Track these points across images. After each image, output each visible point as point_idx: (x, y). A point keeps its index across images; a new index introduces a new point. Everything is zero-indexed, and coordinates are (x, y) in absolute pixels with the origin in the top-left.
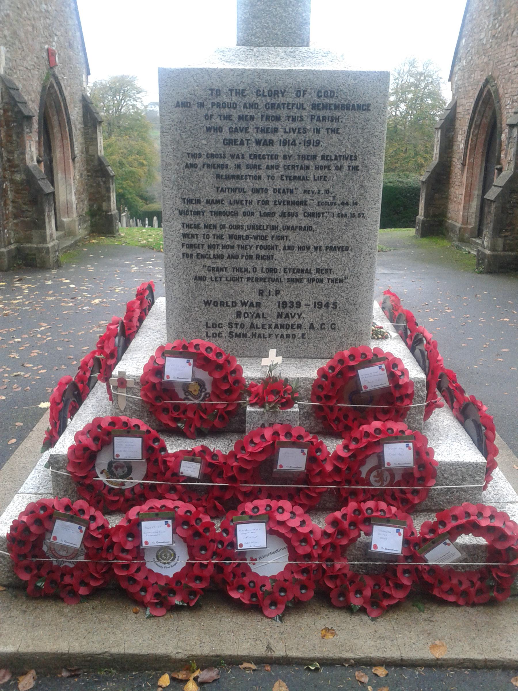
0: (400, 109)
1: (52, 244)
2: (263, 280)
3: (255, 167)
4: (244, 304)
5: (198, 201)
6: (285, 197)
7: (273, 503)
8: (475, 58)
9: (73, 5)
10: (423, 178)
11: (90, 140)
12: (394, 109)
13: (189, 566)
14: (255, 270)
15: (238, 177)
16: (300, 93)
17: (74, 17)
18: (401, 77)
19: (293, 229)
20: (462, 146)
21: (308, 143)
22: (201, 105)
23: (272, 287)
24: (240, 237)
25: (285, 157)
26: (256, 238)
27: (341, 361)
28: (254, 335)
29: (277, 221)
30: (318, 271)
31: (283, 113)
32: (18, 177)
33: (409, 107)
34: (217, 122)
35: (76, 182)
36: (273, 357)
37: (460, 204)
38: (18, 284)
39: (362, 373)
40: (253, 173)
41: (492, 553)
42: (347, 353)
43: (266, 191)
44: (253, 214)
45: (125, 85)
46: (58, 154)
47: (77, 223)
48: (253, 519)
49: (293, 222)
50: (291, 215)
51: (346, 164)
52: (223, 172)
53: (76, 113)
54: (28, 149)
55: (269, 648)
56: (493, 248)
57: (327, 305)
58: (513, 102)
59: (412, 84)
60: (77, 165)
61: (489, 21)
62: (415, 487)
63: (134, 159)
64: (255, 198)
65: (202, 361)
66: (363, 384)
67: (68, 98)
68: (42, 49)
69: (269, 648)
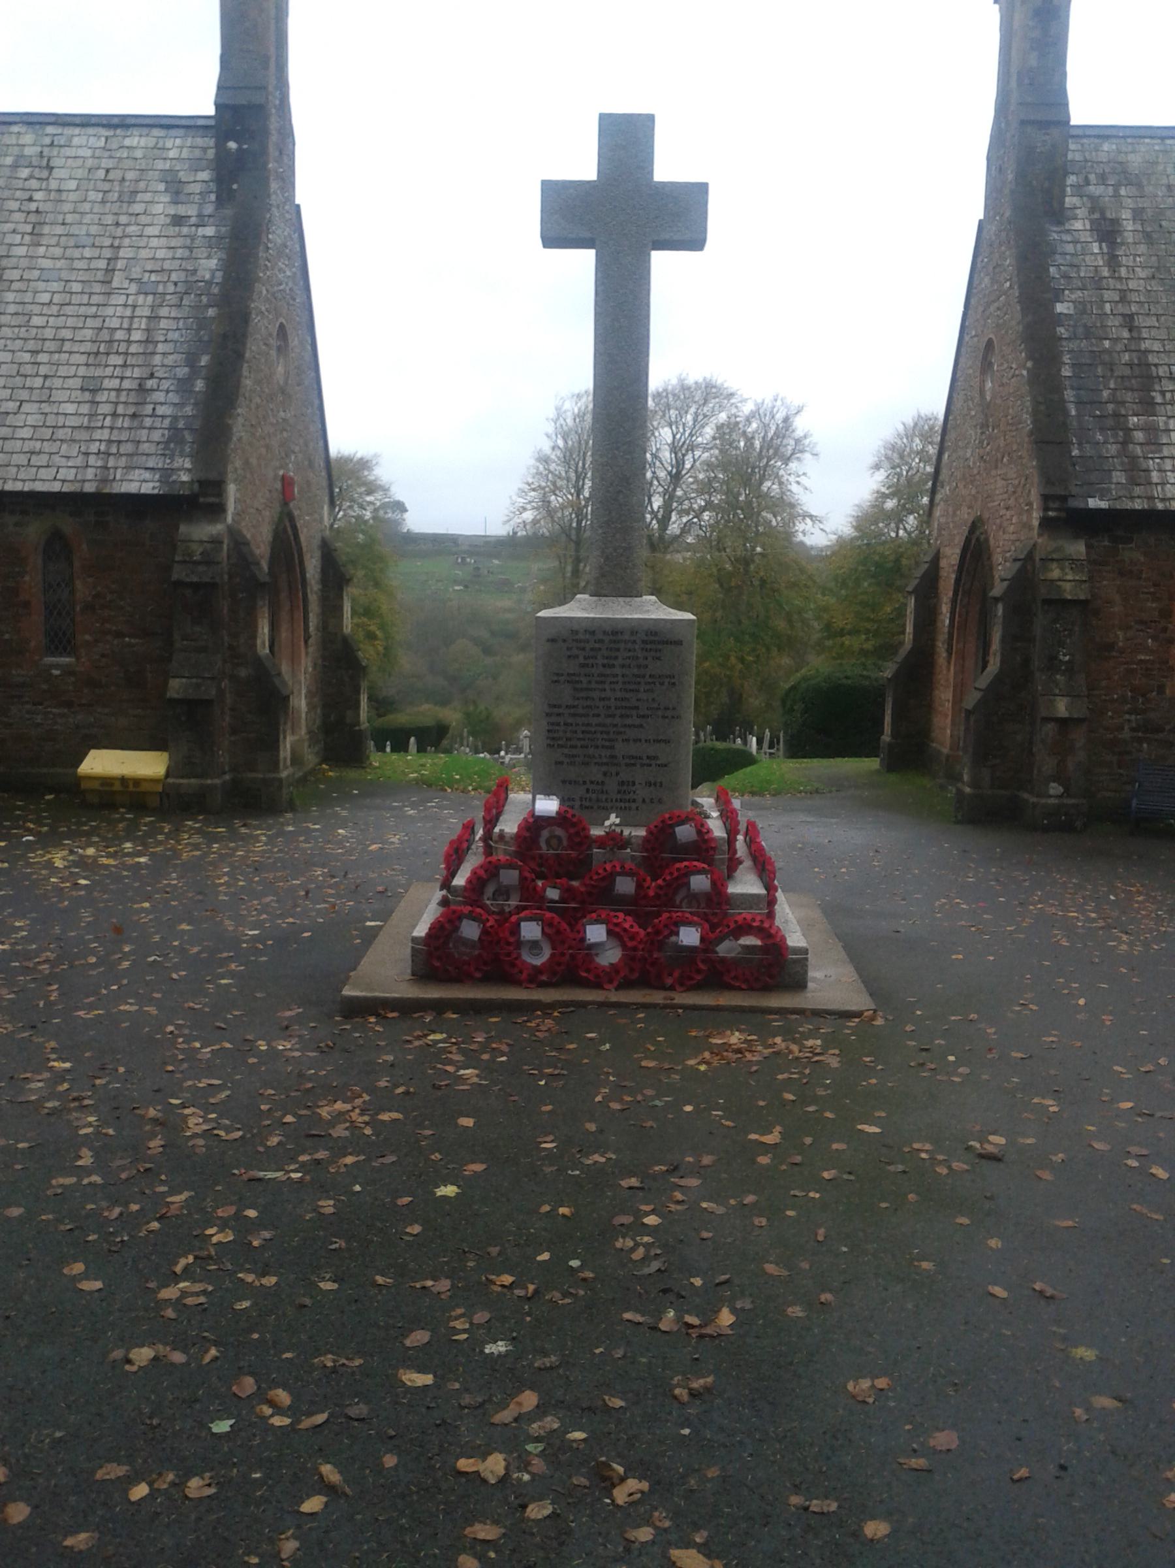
2: (606, 764)
3: (602, 682)
4: (592, 782)
5: (560, 707)
6: (624, 704)
7: (612, 914)
8: (961, 486)
11: (331, 608)
12: (893, 525)
13: (552, 955)
14: (600, 756)
15: (591, 690)
16: (634, 632)
18: (907, 463)
20: (947, 621)
21: (639, 667)
22: (564, 641)
23: (613, 770)
27: (663, 822)
28: (599, 807)
29: (617, 720)
31: (622, 646)
32: (243, 673)
34: (575, 652)
36: (613, 819)
37: (946, 716)
38: (243, 830)
39: (678, 830)
40: (600, 686)
41: (765, 949)
42: (667, 816)
43: (609, 699)
46: (284, 634)
47: (306, 744)
48: (597, 921)
49: (629, 721)
50: (628, 716)
51: (667, 680)
52: (579, 686)
53: (312, 566)
54: (260, 630)
56: (974, 784)
57: (655, 784)
60: (311, 650)
62: (716, 910)
64: (601, 704)
67: (304, 544)
68: (276, 476)
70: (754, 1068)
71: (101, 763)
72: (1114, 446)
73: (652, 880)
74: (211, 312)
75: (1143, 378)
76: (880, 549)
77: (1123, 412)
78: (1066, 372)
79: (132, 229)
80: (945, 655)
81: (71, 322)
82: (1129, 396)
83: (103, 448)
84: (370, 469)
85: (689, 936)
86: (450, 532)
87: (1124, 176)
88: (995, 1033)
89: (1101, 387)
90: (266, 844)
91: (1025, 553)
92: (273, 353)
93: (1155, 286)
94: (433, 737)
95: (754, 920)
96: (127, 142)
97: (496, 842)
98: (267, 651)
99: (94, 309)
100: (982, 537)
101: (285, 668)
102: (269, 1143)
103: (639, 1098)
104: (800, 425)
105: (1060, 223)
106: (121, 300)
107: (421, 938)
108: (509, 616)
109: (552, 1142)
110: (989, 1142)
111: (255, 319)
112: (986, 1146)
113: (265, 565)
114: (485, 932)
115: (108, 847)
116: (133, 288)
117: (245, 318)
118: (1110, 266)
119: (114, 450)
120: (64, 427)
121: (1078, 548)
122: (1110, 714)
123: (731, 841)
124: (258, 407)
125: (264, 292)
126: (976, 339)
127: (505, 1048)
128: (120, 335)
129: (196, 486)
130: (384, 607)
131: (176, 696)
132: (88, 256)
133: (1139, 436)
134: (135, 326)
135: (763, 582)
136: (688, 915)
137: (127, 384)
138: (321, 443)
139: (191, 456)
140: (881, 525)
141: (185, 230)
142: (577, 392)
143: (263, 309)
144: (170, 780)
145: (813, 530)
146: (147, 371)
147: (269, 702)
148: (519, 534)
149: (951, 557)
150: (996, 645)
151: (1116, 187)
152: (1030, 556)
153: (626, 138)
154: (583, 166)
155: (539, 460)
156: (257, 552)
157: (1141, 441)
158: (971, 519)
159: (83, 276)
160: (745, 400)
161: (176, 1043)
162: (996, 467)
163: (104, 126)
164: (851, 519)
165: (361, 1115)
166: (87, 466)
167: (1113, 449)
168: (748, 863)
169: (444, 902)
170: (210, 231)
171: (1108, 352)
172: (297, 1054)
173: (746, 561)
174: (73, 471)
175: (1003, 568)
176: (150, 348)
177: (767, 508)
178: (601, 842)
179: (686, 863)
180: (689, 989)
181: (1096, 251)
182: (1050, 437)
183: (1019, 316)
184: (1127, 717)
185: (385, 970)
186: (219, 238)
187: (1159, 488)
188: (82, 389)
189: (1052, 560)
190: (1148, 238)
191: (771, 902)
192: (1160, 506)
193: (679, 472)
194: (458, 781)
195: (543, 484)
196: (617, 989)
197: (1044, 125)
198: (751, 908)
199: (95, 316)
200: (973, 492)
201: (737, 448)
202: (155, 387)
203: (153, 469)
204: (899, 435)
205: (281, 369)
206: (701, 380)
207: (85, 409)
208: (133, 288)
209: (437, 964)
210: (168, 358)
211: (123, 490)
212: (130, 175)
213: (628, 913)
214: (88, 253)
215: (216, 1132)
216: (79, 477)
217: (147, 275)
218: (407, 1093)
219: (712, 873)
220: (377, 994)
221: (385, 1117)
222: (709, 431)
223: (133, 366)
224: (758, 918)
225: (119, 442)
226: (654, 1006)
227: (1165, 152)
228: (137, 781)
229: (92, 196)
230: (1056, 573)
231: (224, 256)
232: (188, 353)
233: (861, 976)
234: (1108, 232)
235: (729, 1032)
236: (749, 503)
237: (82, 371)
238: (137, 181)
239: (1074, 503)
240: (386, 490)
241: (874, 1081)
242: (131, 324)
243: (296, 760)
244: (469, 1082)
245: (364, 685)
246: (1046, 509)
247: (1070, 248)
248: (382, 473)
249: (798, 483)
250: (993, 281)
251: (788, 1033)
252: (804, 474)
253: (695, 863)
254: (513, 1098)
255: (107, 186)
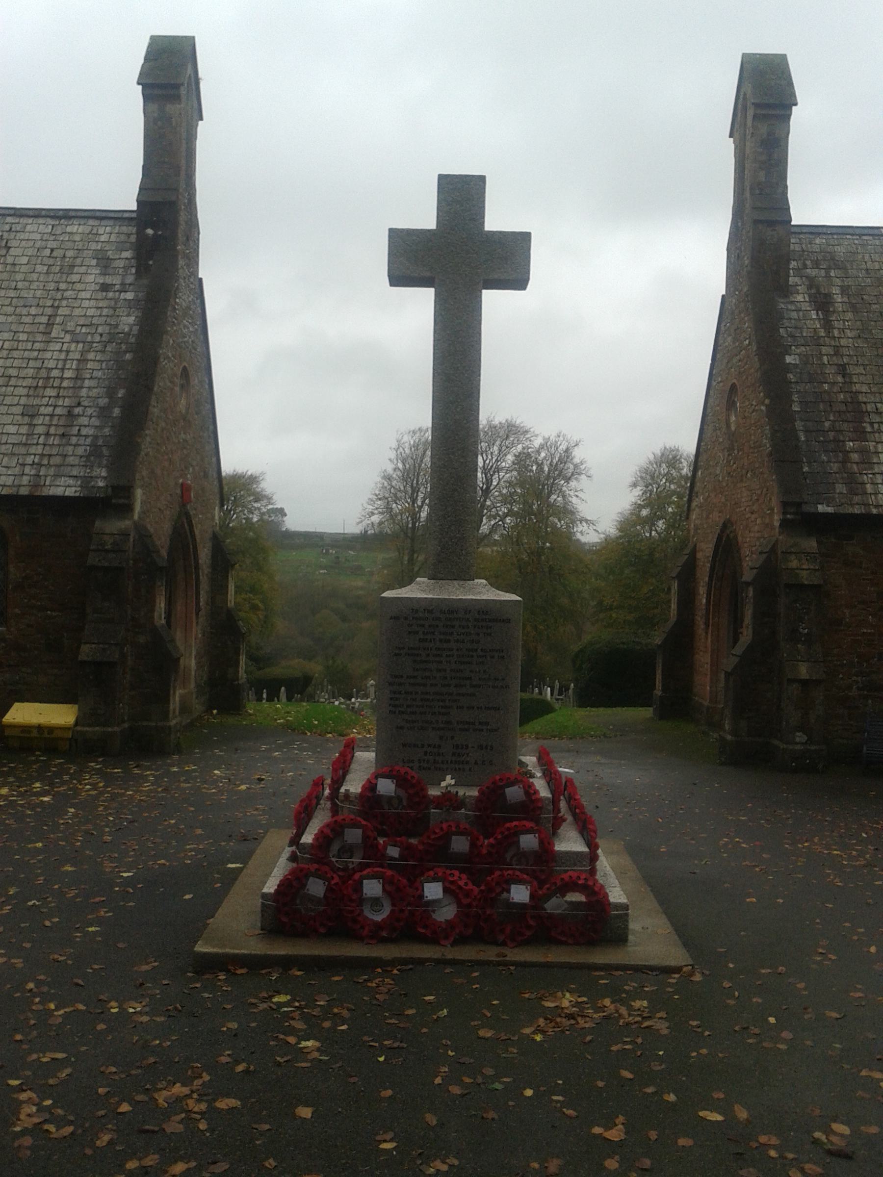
0: (659, 529)
1: (174, 722)
4: (429, 746)
7: (448, 872)
8: (712, 495)
9: (211, 427)
10: (658, 641)
11: (219, 587)
13: (392, 912)
14: (437, 722)
17: (212, 441)
18: (657, 483)
19: (463, 695)
20: (704, 601)
21: (472, 641)
22: (406, 618)
24: (428, 700)
25: (458, 650)
26: (438, 701)
27: (494, 783)
30: (480, 723)
32: (142, 639)
33: (670, 526)
35: (198, 641)
36: (449, 780)
38: (136, 771)
39: (507, 790)
40: (437, 659)
42: (498, 778)
43: (445, 670)
44: (436, 685)
45: (237, 490)
47: (194, 696)
48: (435, 880)
53: (204, 555)
54: (158, 605)
55: (443, 955)
57: (486, 747)
58: (752, 553)
59: (674, 492)
60: (201, 620)
61: (724, 456)
62: (543, 865)
63: (245, 600)
65: (402, 781)
66: (508, 798)
68: (176, 484)
69: (443, 955)
70: (589, 1038)
71: (24, 714)
72: (836, 465)
73: (485, 838)
74: (128, 356)
75: (855, 412)
76: (637, 546)
77: (841, 438)
78: (796, 408)
79: (68, 294)
80: (703, 626)
81: (16, 363)
82: (845, 426)
83: (36, 460)
84: (258, 482)
85: (520, 894)
86: (318, 530)
87: (833, 262)
88: (805, 989)
89: (823, 419)
90: (152, 784)
91: (770, 546)
92: (177, 389)
93: (860, 343)
94: (299, 687)
95: (579, 877)
96: (69, 229)
97: (342, 802)
98: (163, 621)
99: (36, 353)
100: (732, 535)
101: (179, 635)
102: (98, 1143)
103: (480, 1080)
104: (578, 455)
105: (786, 296)
106: (58, 347)
107: (270, 894)
108: (361, 592)
109: (391, 1140)
110: (835, 1133)
111: (164, 362)
112: (833, 1139)
113: (164, 553)
114: (329, 890)
115: (19, 787)
116: (68, 338)
117: (155, 361)
118: (825, 329)
119: (45, 462)
120: (6, 443)
121: (811, 544)
122: (841, 676)
123: (555, 801)
124: (163, 429)
125: (171, 342)
126: (721, 384)
127: (345, 1013)
128: (55, 373)
129: (110, 490)
130: (266, 586)
131: (86, 659)
132: (33, 313)
133: (855, 457)
134: (67, 367)
135: (551, 569)
136: (518, 873)
137: (58, 411)
138: (214, 460)
139: (106, 466)
140: (638, 527)
141: (111, 295)
142: (412, 429)
143: (170, 355)
144: (79, 728)
145: (589, 531)
146: (76, 400)
147: (161, 663)
148: (369, 532)
149: (706, 551)
150: (748, 619)
151: (828, 270)
152: (773, 549)
153: (461, 196)
154: (424, 216)
155: (384, 477)
156: (158, 543)
157: (857, 460)
158: (722, 521)
159: (28, 328)
160: (537, 436)
161: (33, 1003)
162: (742, 481)
163: (52, 217)
164: (616, 523)
165: (199, 1101)
166: (23, 474)
167: (835, 467)
168: (570, 818)
169: (293, 858)
170: (130, 296)
171: (828, 393)
172: (145, 1019)
173: (539, 552)
174: (12, 478)
175: (750, 562)
176: (79, 383)
177: (554, 514)
178: (439, 802)
179: (515, 823)
180: (520, 944)
181: (814, 317)
182: (786, 456)
183: (757, 365)
184: (855, 678)
185: (236, 925)
186: (137, 300)
187: (873, 497)
188: (23, 414)
189: (791, 553)
190: (854, 308)
191: (593, 858)
192: (874, 511)
193: (488, 488)
194: (316, 726)
195: (387, 495)
196: (454, 944)
197: (771, 223)
198: (575, 865)
199: (36, 359)
200: (723, 500)
201: (531, 471)
202: (81, 413)
203: (76, 477)
204: (650, 462)
205: (183, 401)
206: (504, 421)
207: (24, 430)
208: (68, 338)
209: (285, 919)
210: (92, 391)
211: (51, 493)
212: (70, 254)
213: (462, 871)
214: (33, 311)
215: (46, 1127)
216: (16, 483)
217: (79, 328)
218: (246, 1072)
219: (539, 832)
220: (227, 950)
221: (223, 1104)
222: (510, 458)
223: (64, 397)
224: (583, 877)
225: (50, 455)
226: (488, 963)
227: (863, 245)
228: (51, 729)
229: (39, 268)
230: (794, 564)
231: (140, 314)
232: (109, 387)
233: (673, 924)
234: (822, 302)
235: (560, 994)
236: (540, 511)
237: (23, 401)
238: (75, 258)
239: (806, 508)
240: (269, 499)
241: (704, 1051)
242: (64, 365)
243: (185, 709)
244: (310, 1057)
245: (243, 648)
246: (784, 513)
247: (794, 315)
248: (267, 486)
249: (577, 496)
250: (735, 340)
251: (614, 992)
252: (581, 490)
253: (524, 822)
254: (352, 1080)
255: (51, 261)
